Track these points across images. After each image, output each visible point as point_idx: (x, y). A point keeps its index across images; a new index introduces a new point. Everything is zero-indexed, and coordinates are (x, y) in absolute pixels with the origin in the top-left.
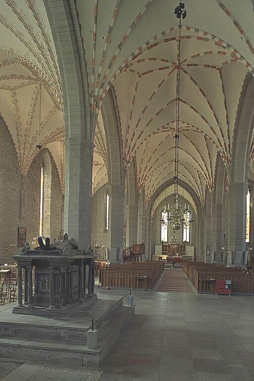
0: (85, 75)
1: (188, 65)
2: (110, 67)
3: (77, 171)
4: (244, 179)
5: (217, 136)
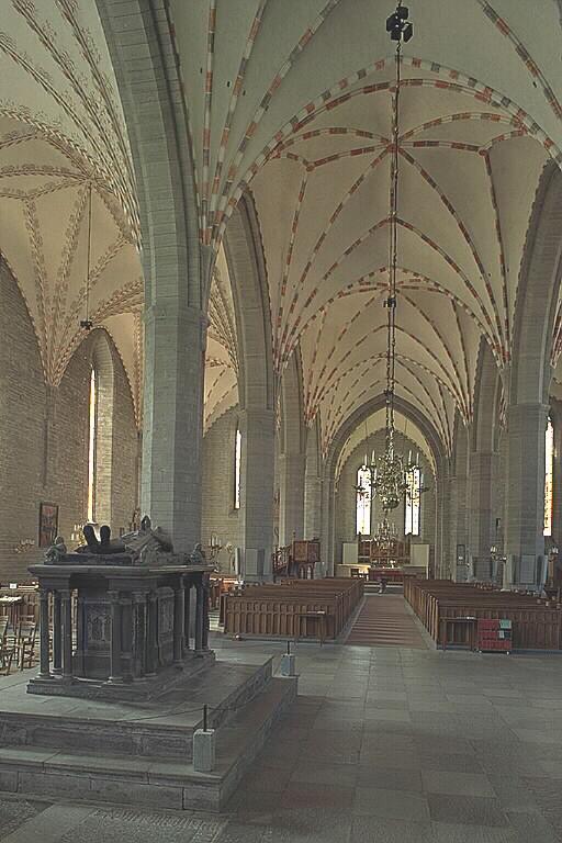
0: (187, 167)
1: (416, 144)
2: (243, 148)
3: (171, 379)
4: (540, 396)
5: (480, 301)
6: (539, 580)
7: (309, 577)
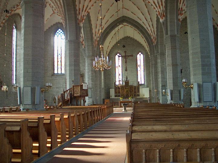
6: (215, 99)
7: (59, 116)
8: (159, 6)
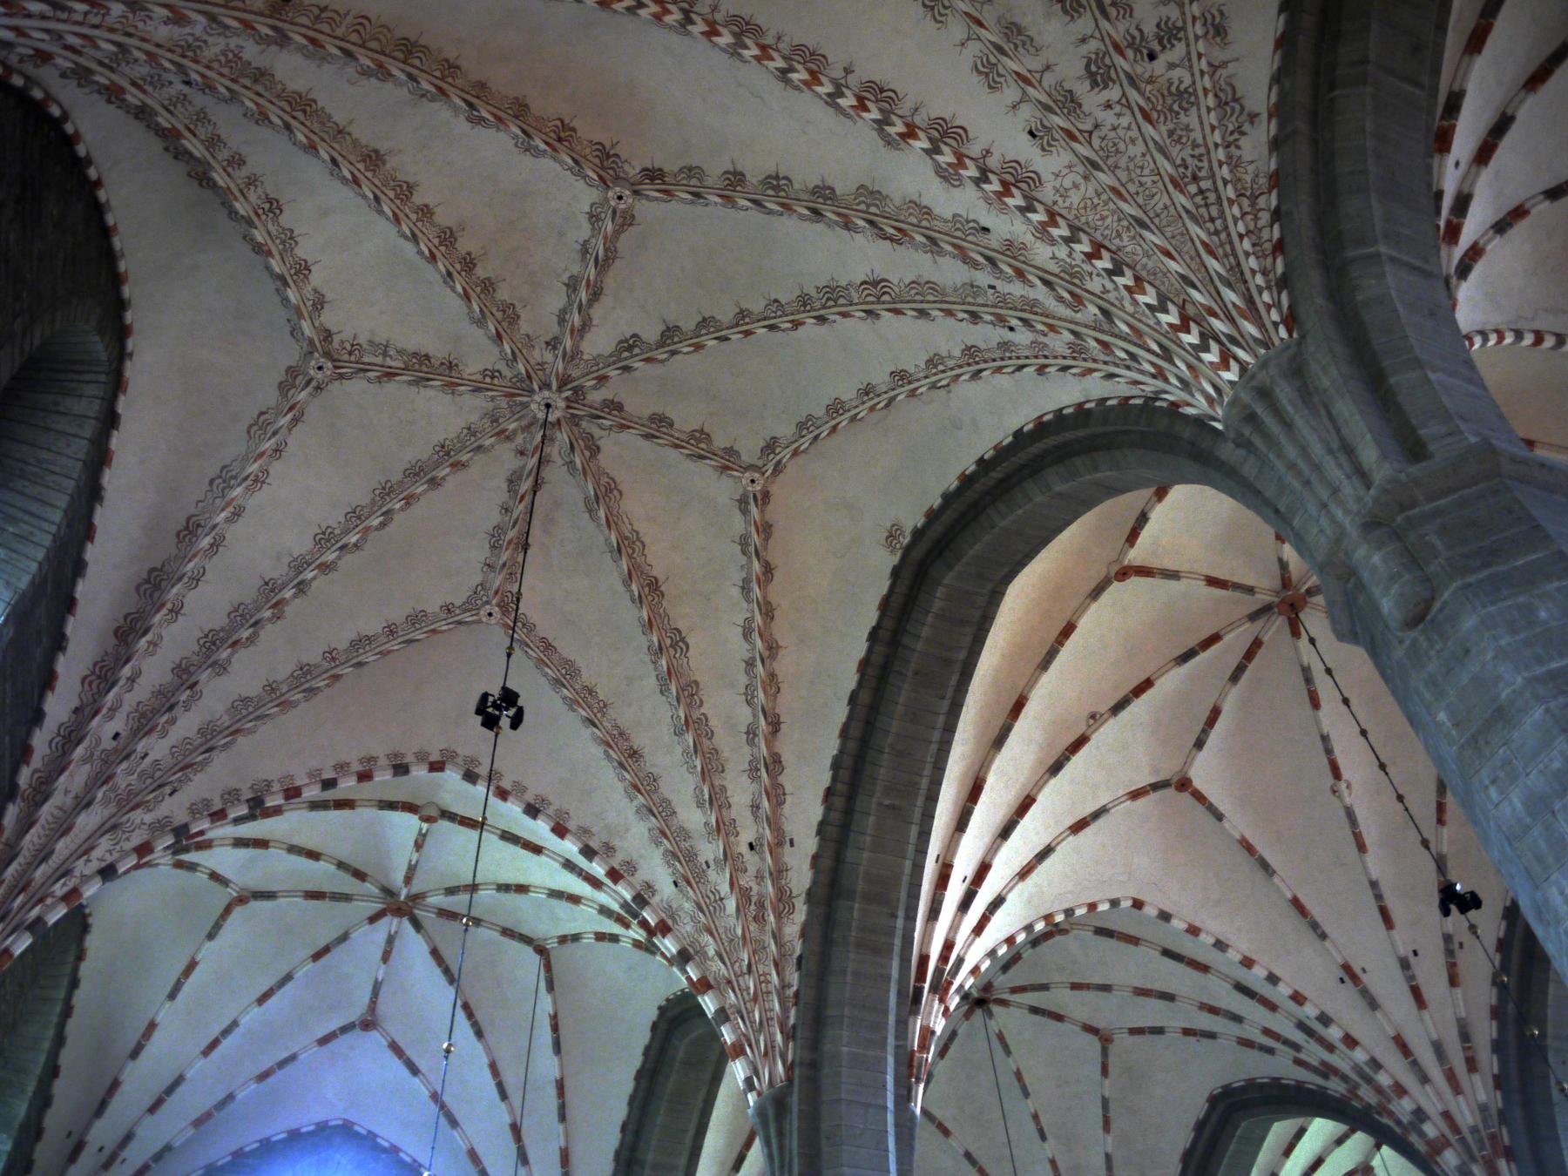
8: (1451, 1077)
